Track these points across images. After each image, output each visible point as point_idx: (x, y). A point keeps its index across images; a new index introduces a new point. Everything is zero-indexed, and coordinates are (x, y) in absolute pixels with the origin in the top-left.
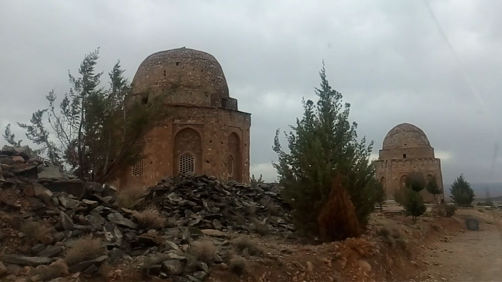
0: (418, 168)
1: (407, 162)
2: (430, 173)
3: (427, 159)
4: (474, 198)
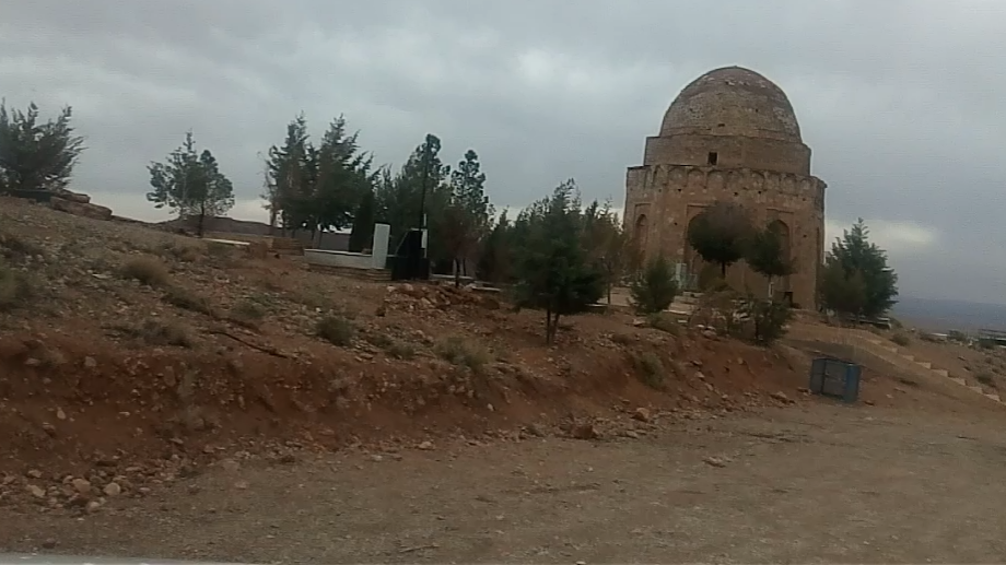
0: (752, 199)
1: (713, 175)
2: (784, 218)
3: (778, 174)
4: (892, 298)
